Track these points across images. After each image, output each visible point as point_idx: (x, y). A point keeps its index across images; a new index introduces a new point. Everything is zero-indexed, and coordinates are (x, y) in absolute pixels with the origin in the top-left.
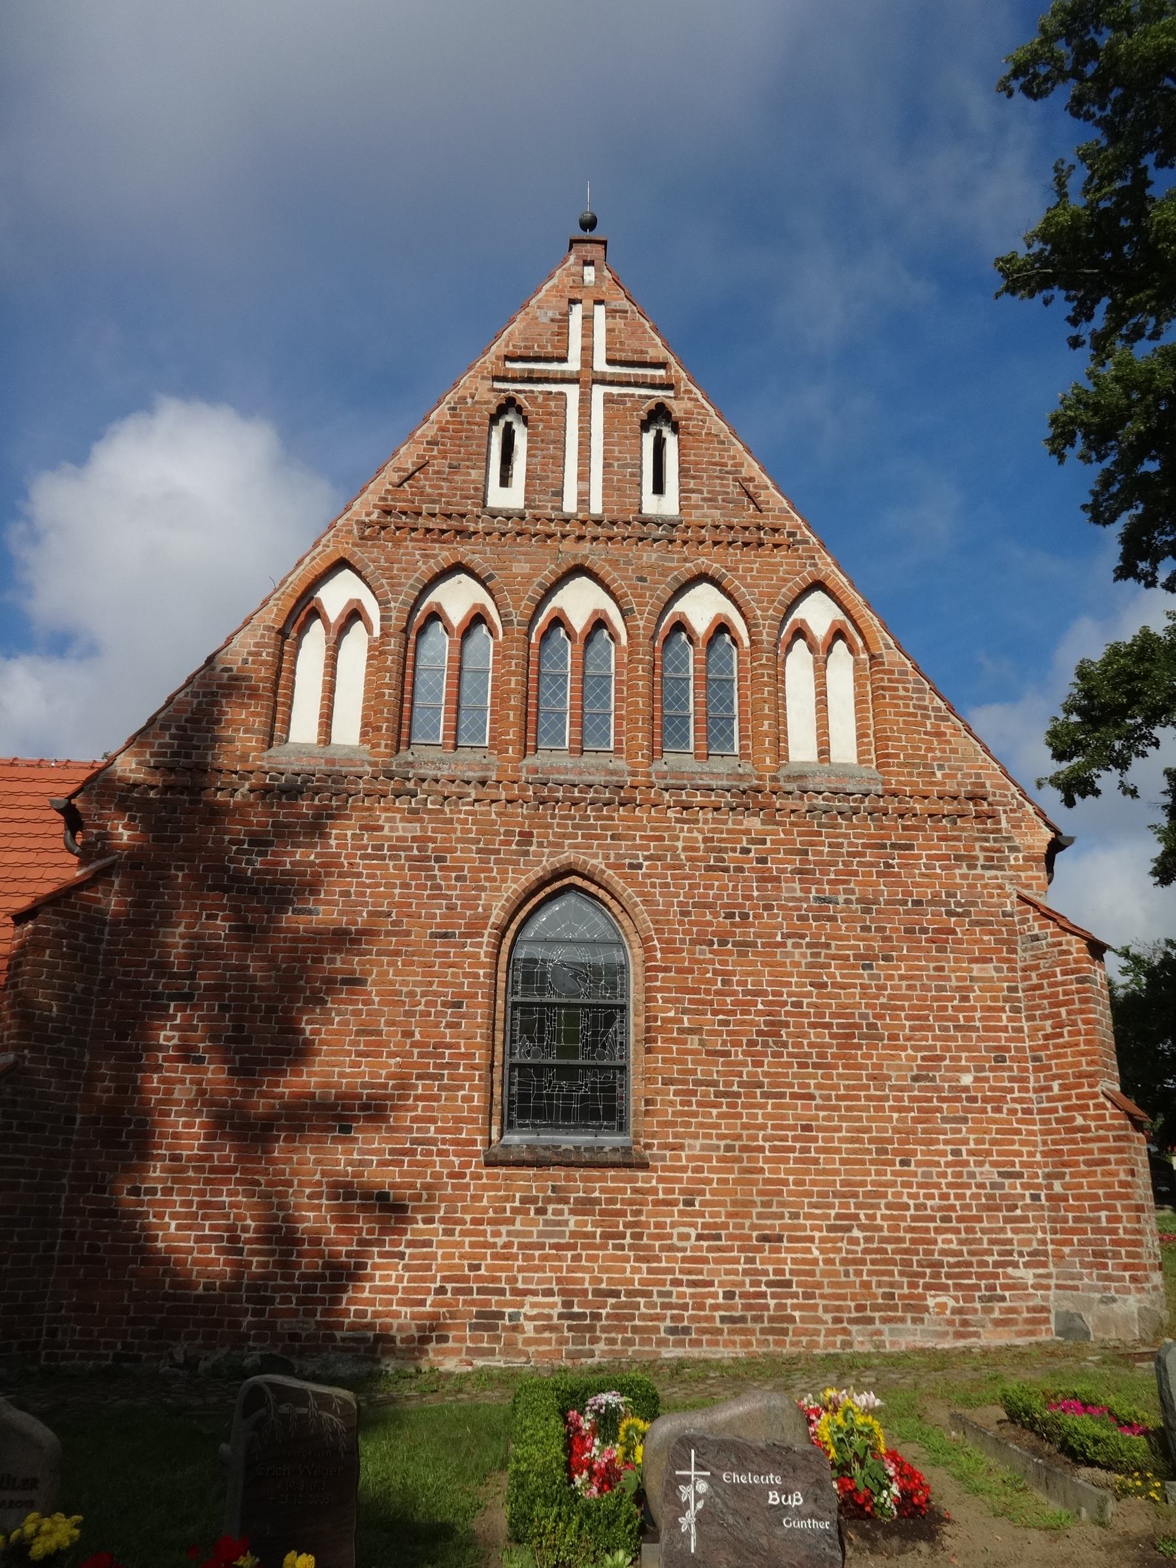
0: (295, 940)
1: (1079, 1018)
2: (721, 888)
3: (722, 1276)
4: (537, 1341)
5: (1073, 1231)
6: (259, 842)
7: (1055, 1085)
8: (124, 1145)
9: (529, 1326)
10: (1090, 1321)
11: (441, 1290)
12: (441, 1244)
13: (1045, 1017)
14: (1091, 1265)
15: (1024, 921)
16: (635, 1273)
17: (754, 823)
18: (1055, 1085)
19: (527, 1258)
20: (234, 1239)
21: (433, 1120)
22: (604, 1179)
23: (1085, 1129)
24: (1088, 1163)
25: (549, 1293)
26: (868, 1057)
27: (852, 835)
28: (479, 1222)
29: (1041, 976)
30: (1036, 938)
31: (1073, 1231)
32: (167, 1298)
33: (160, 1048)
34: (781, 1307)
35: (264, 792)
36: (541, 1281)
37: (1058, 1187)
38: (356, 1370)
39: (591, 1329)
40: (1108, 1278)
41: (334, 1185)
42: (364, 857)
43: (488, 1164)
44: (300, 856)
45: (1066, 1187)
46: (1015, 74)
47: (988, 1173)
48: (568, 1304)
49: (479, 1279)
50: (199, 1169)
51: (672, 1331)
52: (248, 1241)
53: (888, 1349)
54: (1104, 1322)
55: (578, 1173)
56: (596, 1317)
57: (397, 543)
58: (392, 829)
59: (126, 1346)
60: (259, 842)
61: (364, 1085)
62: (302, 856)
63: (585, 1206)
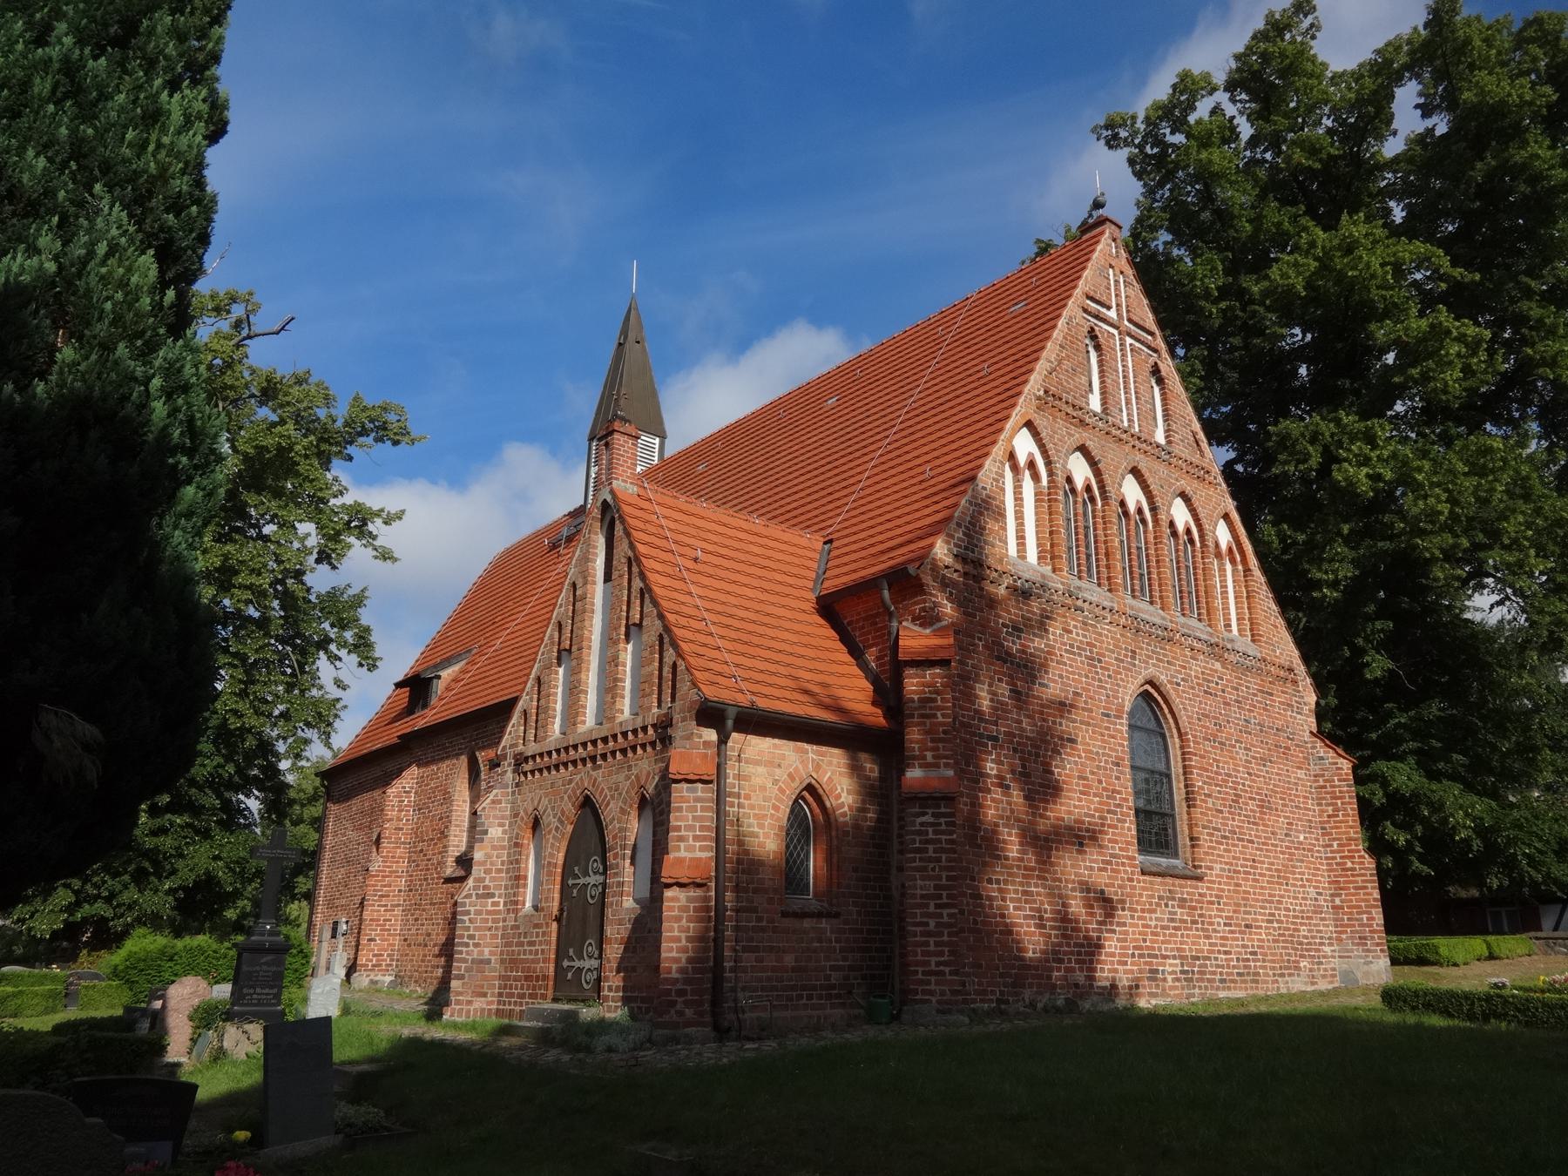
0: (1042, 706)
3: (1235, 946)
4: (1176, 988)
6: (1017, 629)
8: (980, 847)
9: (1169, 978)
10: (1359, 975)
11: (1133, 955)
16: (1204, 945)
17: (1218, 666)
20: (1041, 918)
23: (1353, 869)
25: (1174, 957)
26: (1270, 819)
27: (1253, 683)
30: (1321, 758)
33: (988, 776)
35: (1013, 589)
37: (1337, 901)
38: (848, 1036)
41: (1081, 883)
43: (1143, 873)
44: (1037, 644)
46: (1107, 127)
50: (1019, 867)
52: (1048, 920)
53: (1284, 991)
54: (1367, 974)
57: (1055, 418)
60: (1017, 629)
61: (1087, 815)
62: (1037, 644)
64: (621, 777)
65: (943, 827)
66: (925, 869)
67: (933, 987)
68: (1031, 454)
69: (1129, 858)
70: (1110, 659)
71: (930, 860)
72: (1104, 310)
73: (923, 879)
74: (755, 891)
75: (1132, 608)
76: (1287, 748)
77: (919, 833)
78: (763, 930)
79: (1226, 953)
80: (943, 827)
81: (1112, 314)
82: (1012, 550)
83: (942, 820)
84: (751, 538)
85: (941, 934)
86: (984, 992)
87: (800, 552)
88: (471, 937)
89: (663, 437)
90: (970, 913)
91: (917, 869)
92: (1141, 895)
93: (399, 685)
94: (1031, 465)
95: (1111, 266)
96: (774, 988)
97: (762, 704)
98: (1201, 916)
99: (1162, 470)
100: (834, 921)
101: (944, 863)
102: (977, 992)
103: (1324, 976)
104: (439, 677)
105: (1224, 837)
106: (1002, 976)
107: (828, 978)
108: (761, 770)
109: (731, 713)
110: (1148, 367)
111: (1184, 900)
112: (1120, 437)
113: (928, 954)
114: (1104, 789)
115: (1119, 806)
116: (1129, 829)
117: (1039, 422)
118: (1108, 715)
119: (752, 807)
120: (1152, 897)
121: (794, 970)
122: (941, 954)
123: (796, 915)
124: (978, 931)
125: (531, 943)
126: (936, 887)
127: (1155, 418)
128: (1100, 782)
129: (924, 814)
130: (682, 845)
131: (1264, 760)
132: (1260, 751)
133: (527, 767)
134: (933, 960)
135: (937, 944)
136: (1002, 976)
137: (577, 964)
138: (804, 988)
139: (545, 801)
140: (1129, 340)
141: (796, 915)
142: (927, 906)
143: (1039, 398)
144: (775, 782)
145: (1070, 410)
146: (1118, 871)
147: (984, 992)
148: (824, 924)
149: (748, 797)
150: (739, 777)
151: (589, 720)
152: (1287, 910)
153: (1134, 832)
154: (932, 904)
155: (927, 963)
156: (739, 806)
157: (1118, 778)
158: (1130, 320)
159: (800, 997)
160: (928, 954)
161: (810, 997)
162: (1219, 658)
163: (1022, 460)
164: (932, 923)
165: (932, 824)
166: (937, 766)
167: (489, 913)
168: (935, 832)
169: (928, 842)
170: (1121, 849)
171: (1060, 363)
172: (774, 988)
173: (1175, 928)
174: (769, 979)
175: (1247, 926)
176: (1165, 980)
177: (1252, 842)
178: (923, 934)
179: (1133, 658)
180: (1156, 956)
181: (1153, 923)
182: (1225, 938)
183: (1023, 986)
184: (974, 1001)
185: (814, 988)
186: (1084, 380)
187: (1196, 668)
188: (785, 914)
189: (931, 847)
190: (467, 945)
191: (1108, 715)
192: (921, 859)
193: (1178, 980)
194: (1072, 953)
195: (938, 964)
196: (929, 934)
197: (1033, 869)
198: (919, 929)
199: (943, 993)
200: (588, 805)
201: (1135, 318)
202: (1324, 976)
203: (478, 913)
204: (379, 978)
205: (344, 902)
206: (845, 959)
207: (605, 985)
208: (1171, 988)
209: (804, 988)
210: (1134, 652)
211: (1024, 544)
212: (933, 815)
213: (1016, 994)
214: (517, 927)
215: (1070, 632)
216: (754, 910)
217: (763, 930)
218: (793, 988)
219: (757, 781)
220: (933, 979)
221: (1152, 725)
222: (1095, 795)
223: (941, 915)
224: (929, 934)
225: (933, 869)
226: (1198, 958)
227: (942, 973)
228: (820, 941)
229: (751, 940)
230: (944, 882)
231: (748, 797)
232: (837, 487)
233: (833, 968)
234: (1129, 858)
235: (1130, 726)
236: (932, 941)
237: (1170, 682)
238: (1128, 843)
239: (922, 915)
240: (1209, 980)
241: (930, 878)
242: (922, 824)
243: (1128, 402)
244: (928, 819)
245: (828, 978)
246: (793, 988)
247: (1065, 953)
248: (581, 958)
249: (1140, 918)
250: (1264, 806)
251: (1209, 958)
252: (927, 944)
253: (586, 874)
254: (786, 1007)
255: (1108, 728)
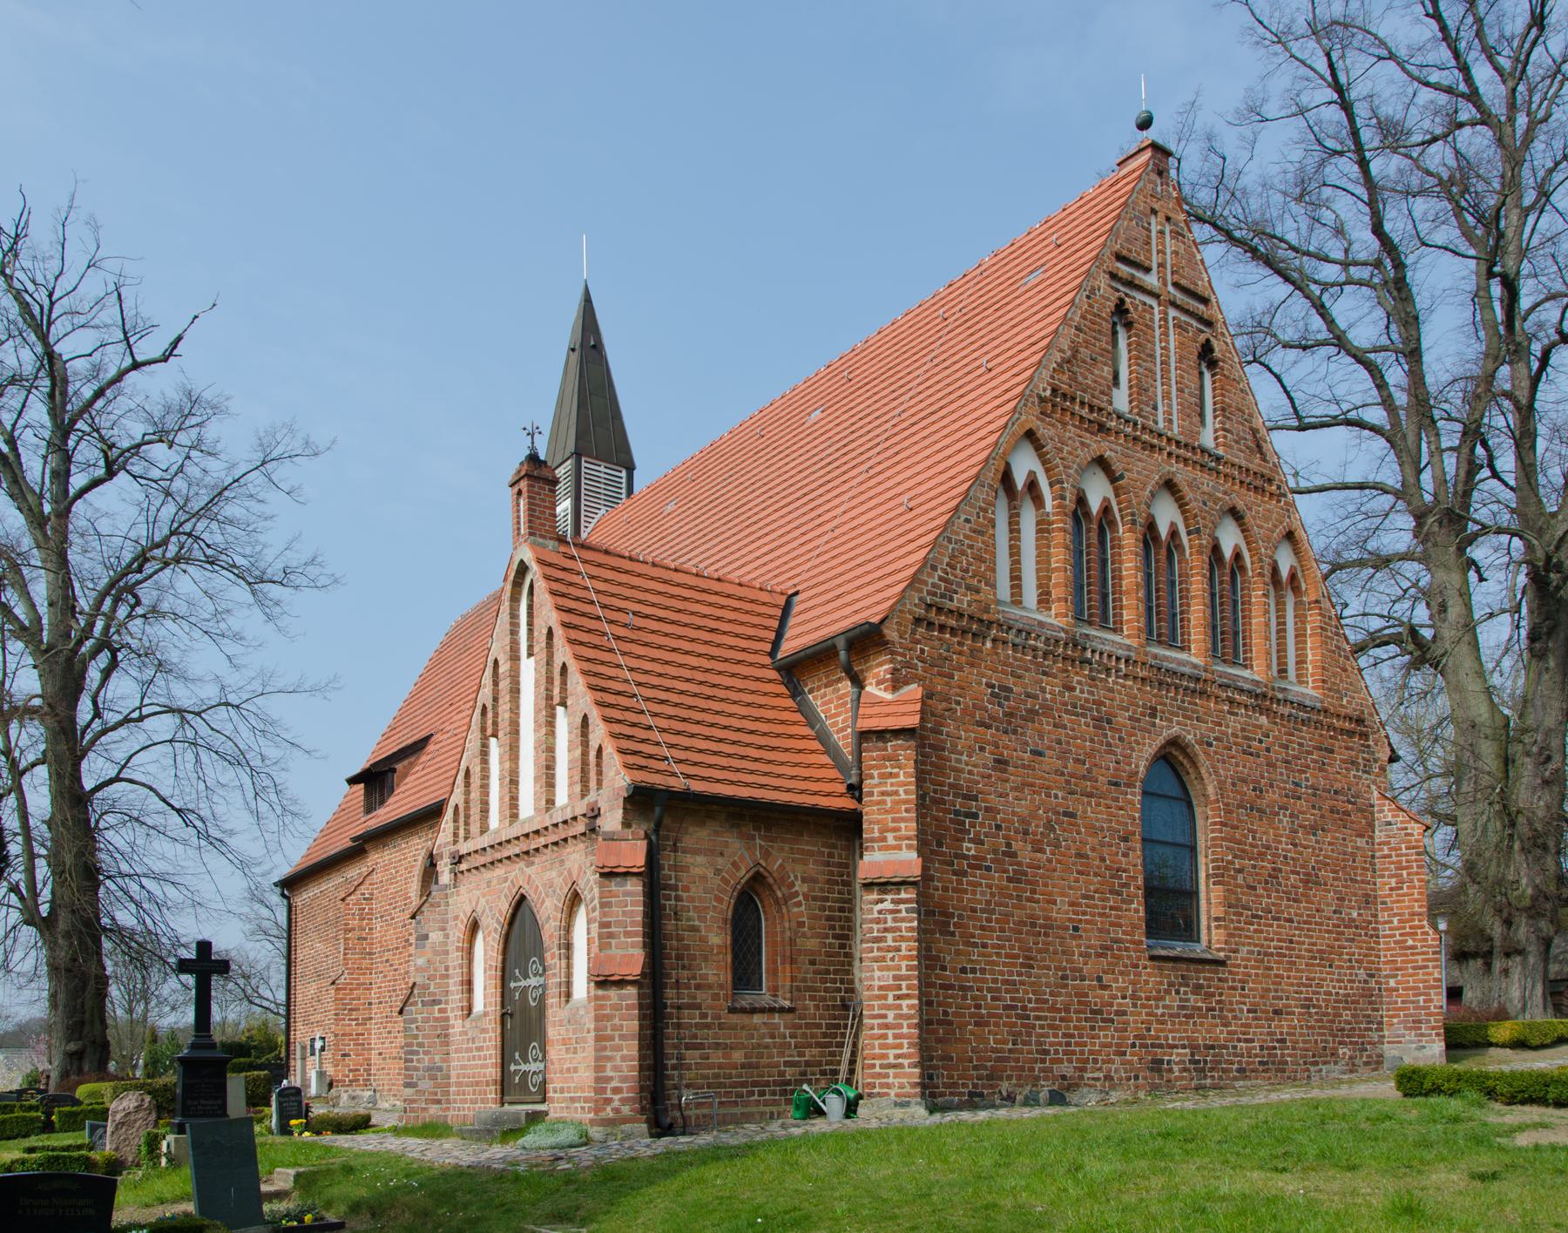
1: (1415, 878)
2: (1247, 766)
3: (1259, 1032)
4: (1182, 1078)
5: (1400, 1009)
7: (1395, 920)
8: (953, 934)
9: (1176, 1068)
11: (1133, 1045)
12: (1132, 1014)
13: (1391, 876)
14: (1410, 1029)
15: (1381, 811)
16: (1221, 1033)
17: (1263, 720)
18: (1395, 920)
19: (1174, 1023)
21: (1120, 926)
22: (1203, 971)
24: (1414, 968)
25: (1184, 1047)
27: (1307, 736)
28: (1148, 999)
29: (1391, 849)
30: (1389, 824)
31: (1400, 1009)
32: (993, 1050)
34: (1283, 1055)
36: (1181, 1039)
39: (1203, 1070)
40: (1422, 1035)
42: (1067, 712)
45: (1398, 983)
47: (1362, 974)
48: (1193, 1055)
49: (1151, 1037)
51: (1239, 1070)
55: (1192, 967)
56: (1205, 1062)
58: (1082, 692)
59: (975, 1086)
63: (1197, 989)
64: (554, 874)
65: (904, 914)
66: (883, 959)
67: (890, 1080)
68: (1032, 474)
69: (1133, 942)
70: (1122, 718)
71: (889, 949)
72: (1139, 274)
73: (880, 969)
74: (698, 987)
75: (1155, 657)
76: (1347, 813)
77: (878, 921)
78: (707, 1026)
79: (1247, 1041)
80: (904, 914)
81: (1151, 280)
82: (1004, 590)
83: (902, 907)
84: (698, 596)
85: (900, 1026)
86: (955, 1085)
87: (763, 609)
88: (421, 1045)
89: (630, 469)
90: (939, 1004)
91: (876, 960)
92: (1147, 982)
93: (352, 781)
94: (1032, 485)
95: (1154, 212)
96: (720, 1085)
97: (697, 786)
98: (1219, 1002)
99: (1207, 482)
100: (791, 1016)
101: (904, 952)
102: (946, 1085)
103: (1366, 1064)
104: (394, 770)
105: (1256, 916)
106: (976, 1068)
107: (782, 1074)
108: (700, 859)
109: (841, 643)
110: (1195, 348)
111: (1200, 986)
112: (1148, 440)
113: (887, 1046)
114: (1107, 868)
115: (1126, 885)
116: (1137, 911)
117: (1044, 431)
118: (1116, 784)
119: (692, 899)
120: (1161, 983)
121: (743, 1066)
122: (900, 1046)
123: (743, 1010)
124: (950, 1023)
125: (479, 1049)
126: (895, 978)
127: (1202, 415)
128: (1103, 859)
129: (882, 901)
130: (613, 942)
131: (1313, 829)
132: (1310, 817)
133: (463, 867)
134: (892, 1052)
135: (896, 1036)
136: (976, 1068)
137: (523, 1067)
138: (755, 1084)
139: (483, 901)
140: (1172, 313)
141: (743, 1010)
142: (885, 997)
143: (1042, 400)
144: (718, 872)
145: (1085, 412)
146: (1120, 958)
147: (955, 1085)
148: (777, 1019)
149: (686, 889)
150: (675, 868)
151: (527, 807)
152: (1330, 994)
153: (1142, 914)
154: (891, 995)
155: (885, 1056)
156: (678, 898)
157: (1125, 855)
158: (1175, 285)
159: (752, 1093)
160: (887, 1046)
161: (762, 1094)
162: (1267, 711)
163: (1020, 480)
164: (891, 1014)
165: (892, 912)
166: (899, 848)
167: (436, 1019)
168: (895, 920)
169: (886, 930)
170: (1124, 933)
171: (1075, 352)
172: (720, 1085)
173: (1185, 1016)
174: (717, 1076)
175: (1276, 1012)
176: (1170, 1070)
177: (1291, 921)
178: (881, 1026)
179: (1153, 715)
180: (1161, 1046)
181: (1160, 1011)
182: (1249, 1026)
183: (1001, 1079)
184: (942, 1095)
185: (767, 1084)
186: (1107, 371)
187: (1233, 724)
188: (732, 1010)
189: (890, 936)
190: (417, 1053)
191: (1116, 784)
192: (879, 949)
193: (1185, 1070)
194: (1060, 1044)
195: (897, 1057)
196: (887, 1026)
197: (1016, 957)
198: (876, 1022)
199: (901, 1086)
200: (521, 902)
201: (1183, 282)
202: (1366, 1064)
203: (426, 1020)
204: (359, 1093)
205: (318, 1017)
206: (801, 1054)
207: (550, 1087)
208: (1177, 1079)
209: (755, 1084)
210: (1154, 709)
211: (1019, 586)
212: (893, 901)
213: (992, 1086)
214: (465, 1033)
215: (1073, 689)
216: (699, 1007)
217: (707, 1026)
218: (743, 1085)
219: (698, 871)
220: (891, 1071)
221: (1175, 791)
222: (1096, 875)
223: (899, 1007)
224: (887, 1026)
225: (892, 959)
226: (1213, 1047)
227: (901, 1066)
228: (773, 1036)
229: (695, 1037)
230: (904, 972)
231: (686, 889)
232: (811, 525)
233: (786, 1064)
234: (1133, 942)
235: (1144, 793)
236: (890, 1032)
237: (1200, 743)
238: (1134, 926)
239: (881, 1007)
240: (1224, 1071)
241: (888, 968)
242: (880, 912)
243: (1166, 395)
244: (887, 905)
245: (782, 1074)
246: (743, 1085)
247: (1051, 1044)
248: (526, 1061)
249: (1143, 1006)
250: (1310, 880)
251: (1226, 1047)
252: (885, 1036)
253: (526, 976)
254: (736, 1103)
255: (1117, 800)
